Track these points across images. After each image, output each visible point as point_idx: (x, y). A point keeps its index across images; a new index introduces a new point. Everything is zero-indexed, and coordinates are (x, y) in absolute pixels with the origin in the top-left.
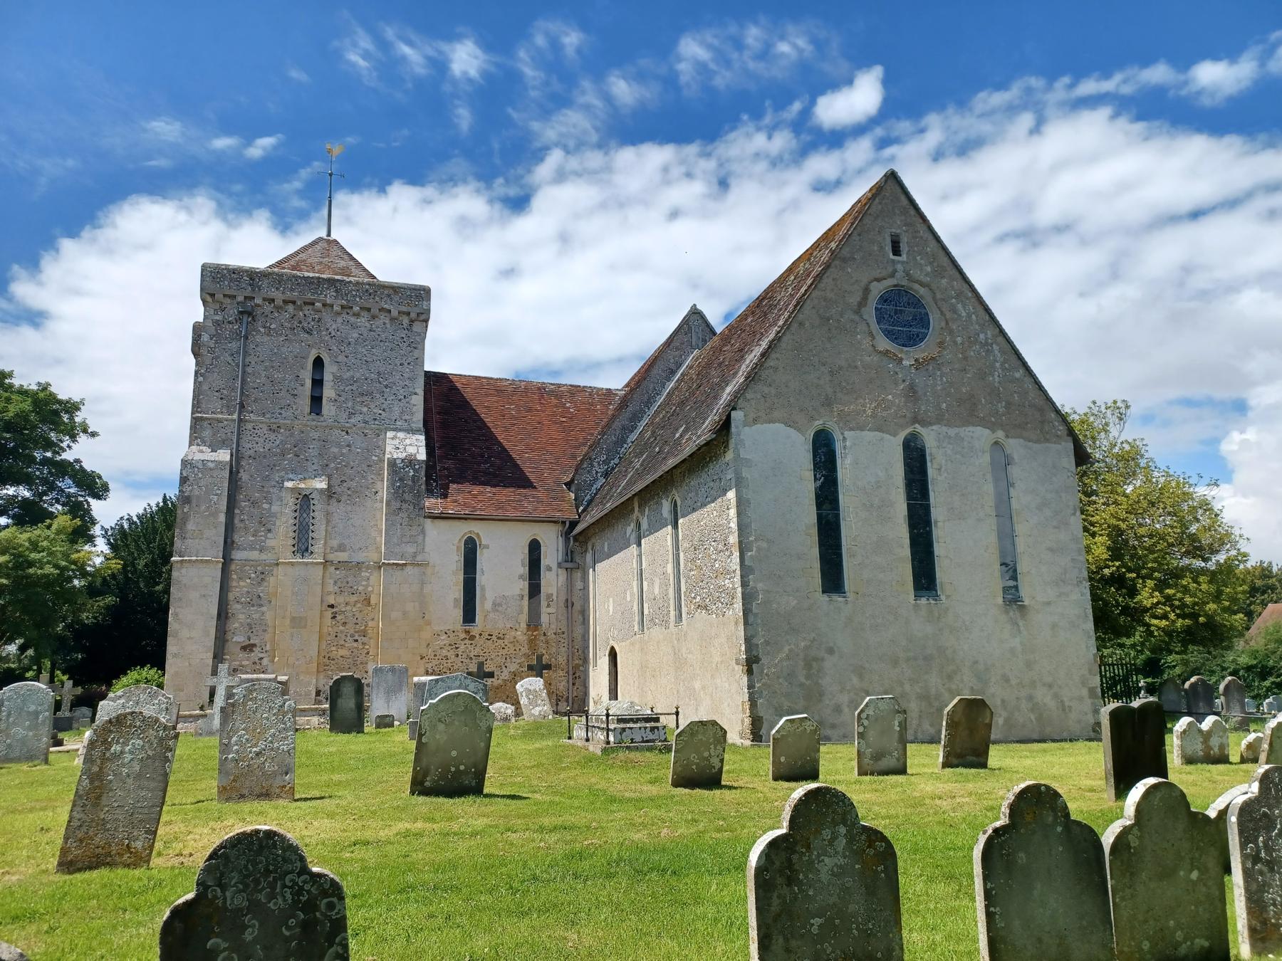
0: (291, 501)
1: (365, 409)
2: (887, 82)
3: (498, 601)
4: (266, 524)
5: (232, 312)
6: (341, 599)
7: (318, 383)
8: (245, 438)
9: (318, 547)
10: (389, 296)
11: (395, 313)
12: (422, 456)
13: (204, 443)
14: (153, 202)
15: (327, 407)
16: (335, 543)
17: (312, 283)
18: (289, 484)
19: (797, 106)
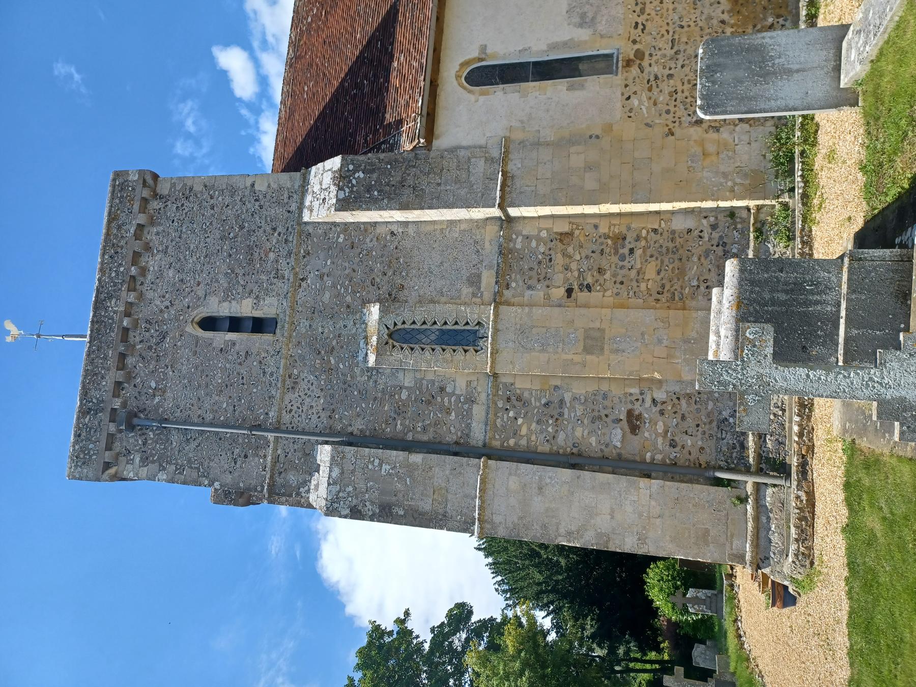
0: (397, 355)
1: (272, 256)
2: (227, 44)
3: (577, 20)
4: (432, 395)
5: (132, 440)
6: (558, 279)
7: (235, 324)
8: (303, 424)
9: (470, 314)
10: (119, 227)
11: (142, 219)
12: (335, 162)
13: (306, 482)
14: (321, 557)
15: (268, 308)
16: (466, 291)
17: (98, 330)
18: (372, 359)
19: (244, 112)
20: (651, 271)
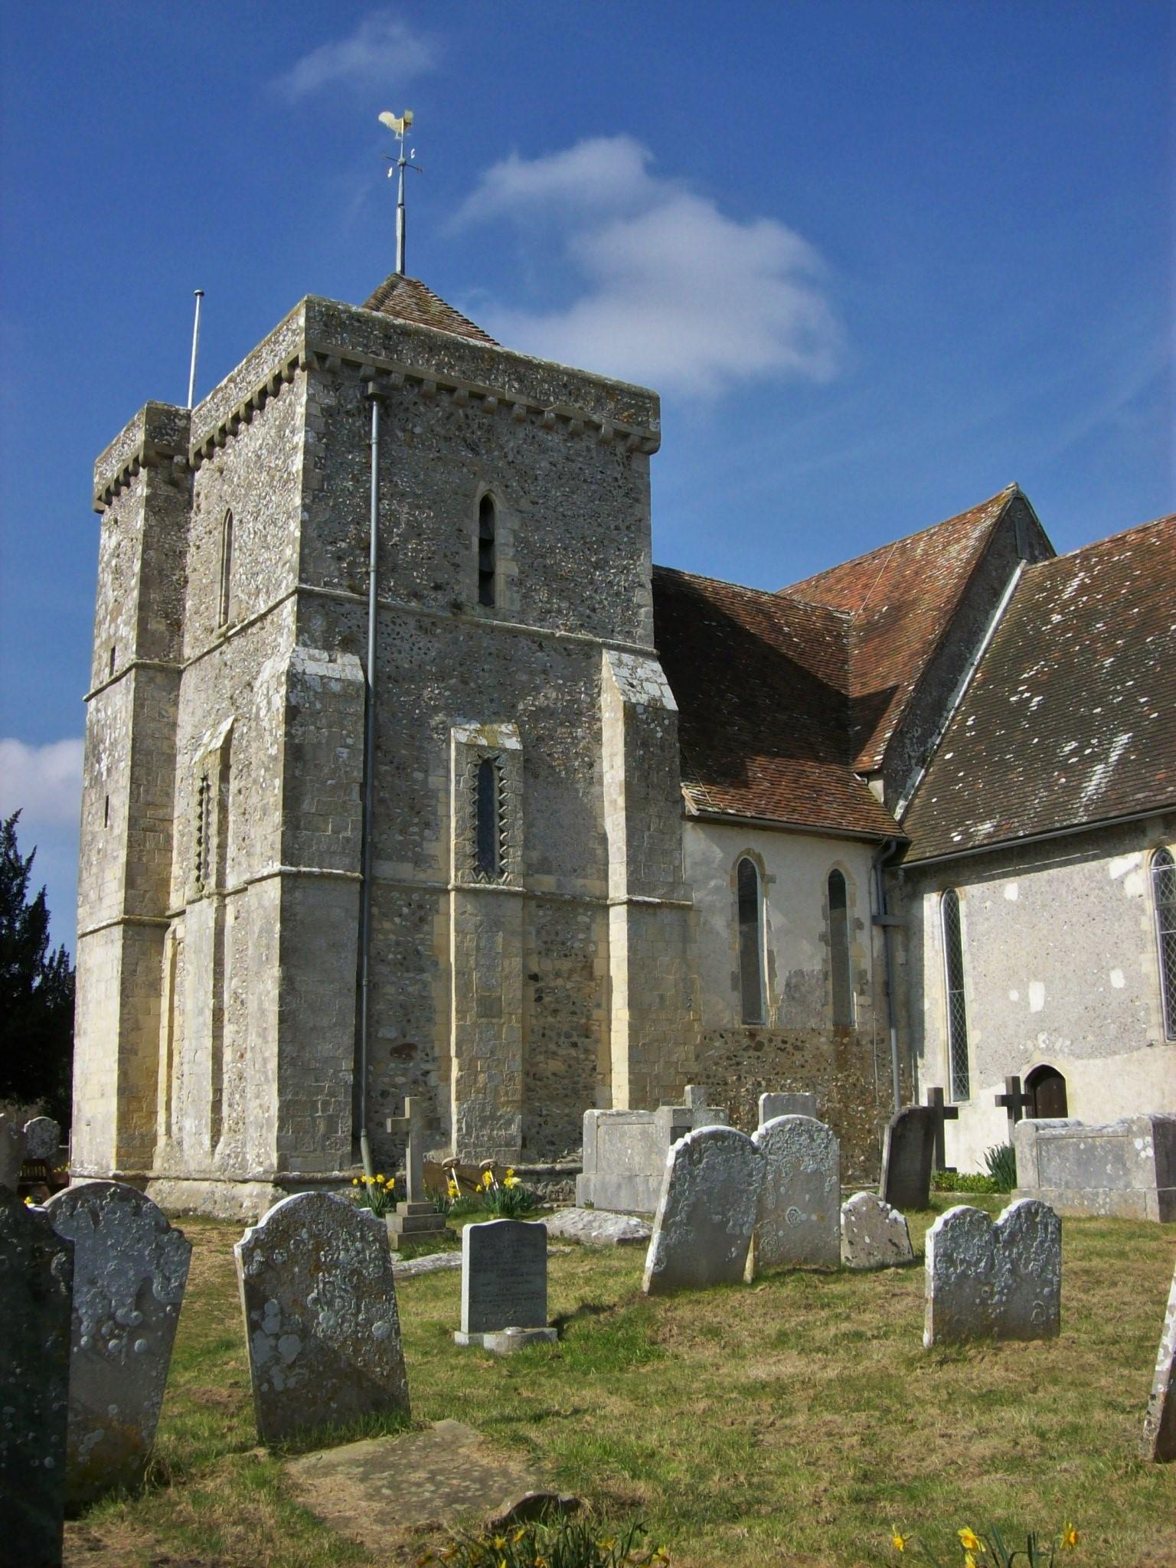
6: (547, 965)
20: (555, 1065)
